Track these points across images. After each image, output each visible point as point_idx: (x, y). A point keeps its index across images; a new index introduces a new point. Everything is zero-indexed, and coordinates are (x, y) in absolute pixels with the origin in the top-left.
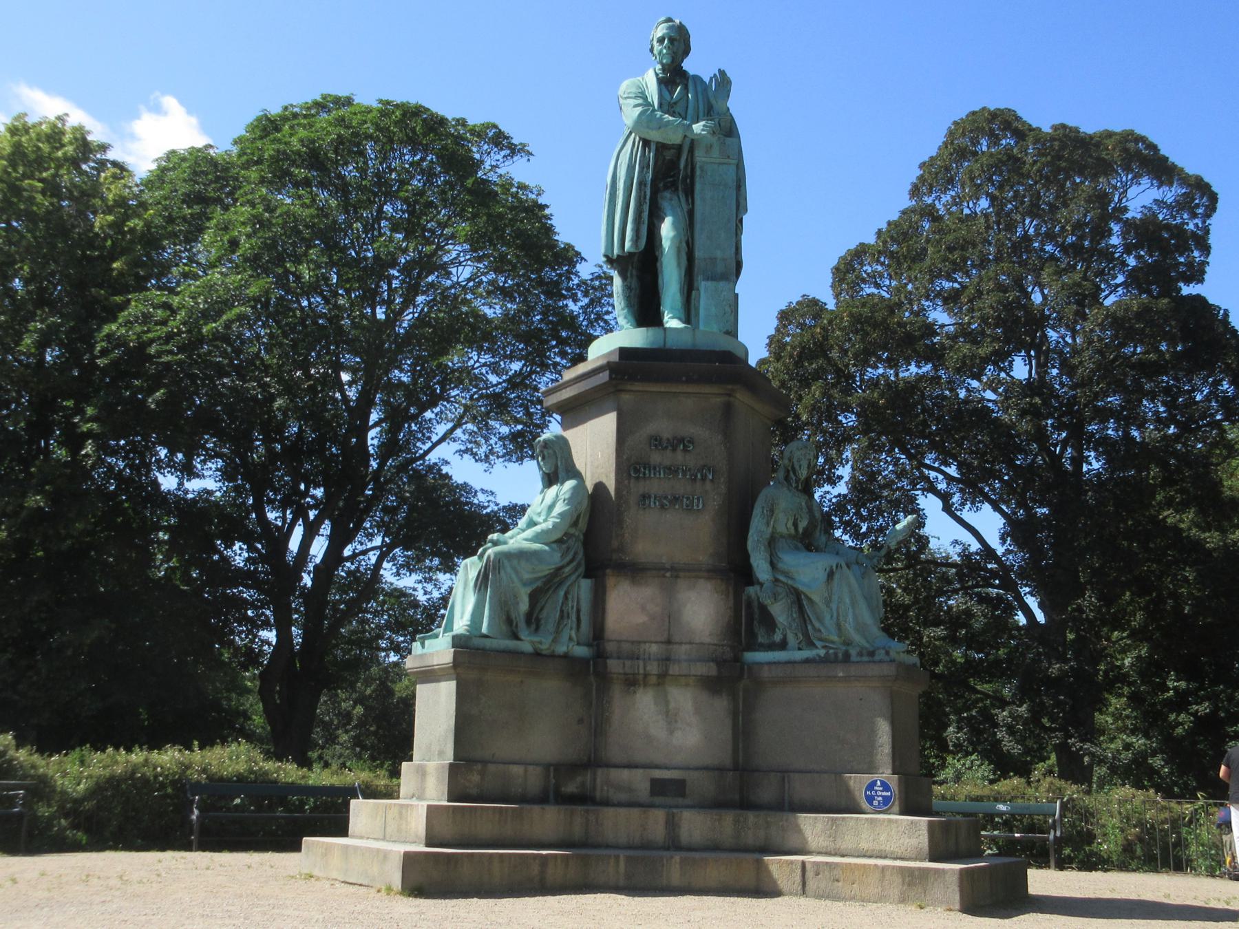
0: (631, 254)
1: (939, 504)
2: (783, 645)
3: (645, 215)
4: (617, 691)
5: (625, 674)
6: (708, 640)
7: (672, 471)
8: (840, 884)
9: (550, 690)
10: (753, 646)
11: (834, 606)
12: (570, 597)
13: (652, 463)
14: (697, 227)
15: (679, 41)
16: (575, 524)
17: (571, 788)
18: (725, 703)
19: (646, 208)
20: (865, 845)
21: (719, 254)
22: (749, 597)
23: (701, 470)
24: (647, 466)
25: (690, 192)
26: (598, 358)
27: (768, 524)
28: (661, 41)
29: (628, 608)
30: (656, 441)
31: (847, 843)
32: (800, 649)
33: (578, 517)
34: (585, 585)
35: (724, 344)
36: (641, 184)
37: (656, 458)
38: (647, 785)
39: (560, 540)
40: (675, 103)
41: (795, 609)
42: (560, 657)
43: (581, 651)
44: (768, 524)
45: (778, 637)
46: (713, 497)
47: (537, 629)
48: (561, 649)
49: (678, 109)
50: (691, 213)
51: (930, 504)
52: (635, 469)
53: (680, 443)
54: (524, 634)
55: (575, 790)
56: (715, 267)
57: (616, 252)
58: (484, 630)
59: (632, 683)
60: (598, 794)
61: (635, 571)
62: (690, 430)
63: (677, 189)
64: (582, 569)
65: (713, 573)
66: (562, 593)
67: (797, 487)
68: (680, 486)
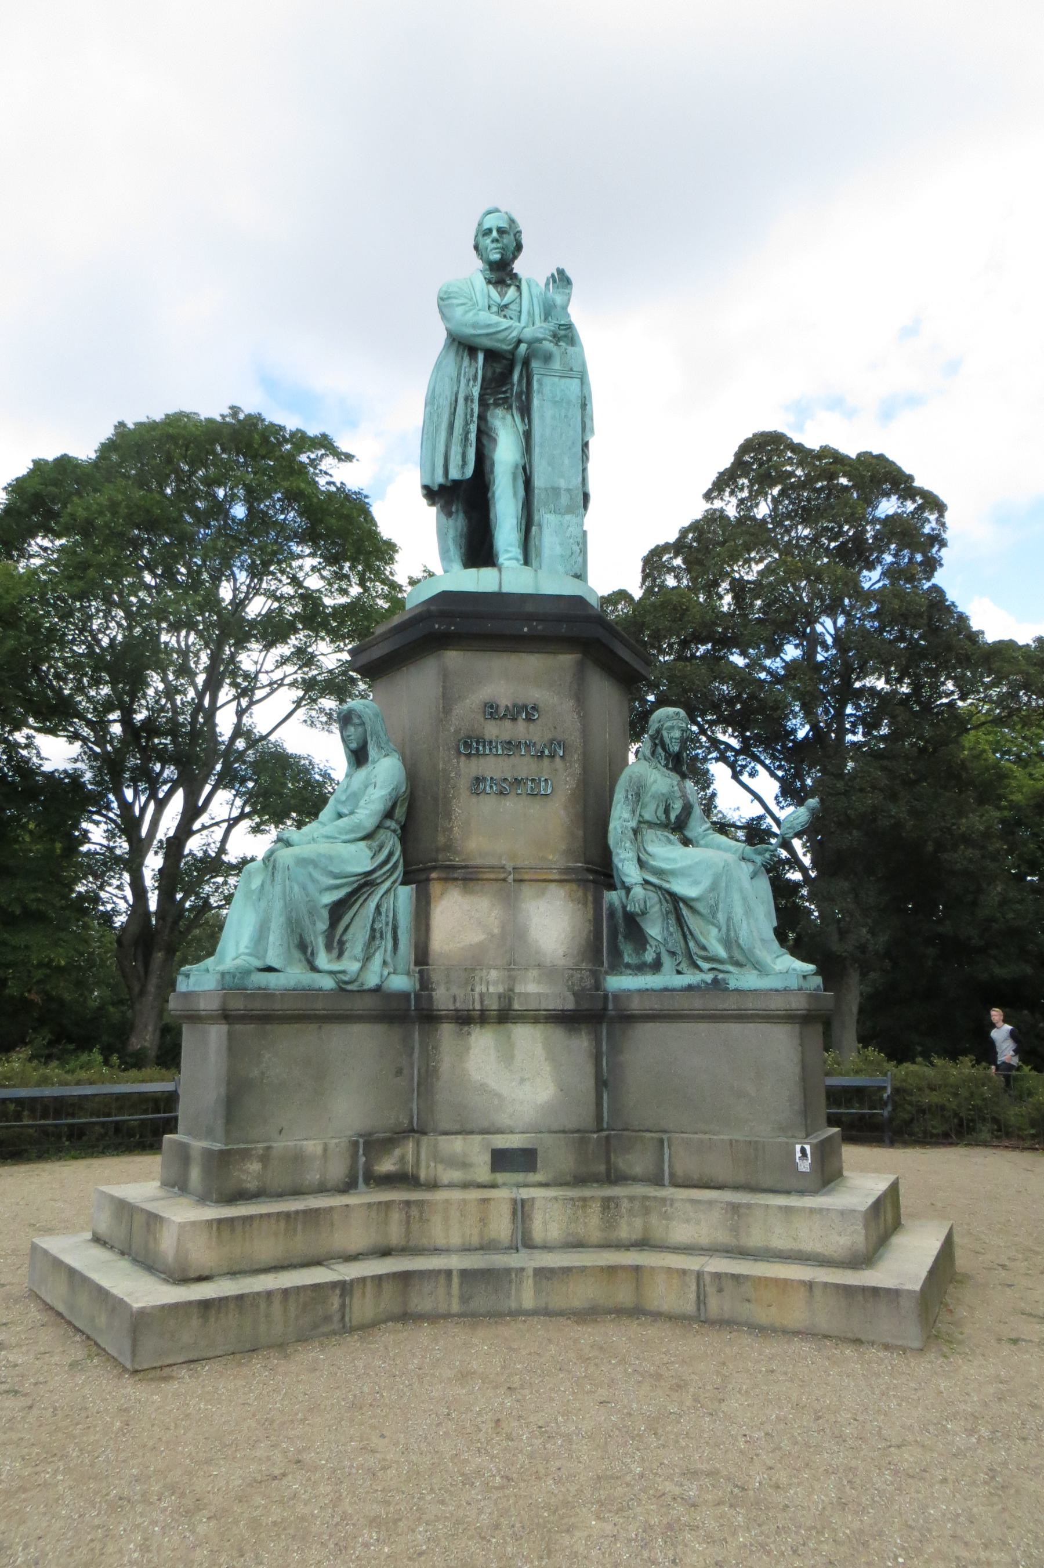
0: (455, 482)
1: (729, 772)
2: (656, 966)
3: (473, 437)
5: (456, 1010)
6: (562, 962)
7: (512, 746)
10: (617, 966)
11: (721, 917)
12: (383, 910)
13: (487, 738)
14: (537, 451)
17: (387, 1166)
19: (473, 428)
20: (779, 1241)
21: (562, 483)
22: (611, 905)
25: (526, 411)
26: (417, 606)
27: (633, 812)
29: (459, 921)
31: (755, 1238)
32: (679, 972)
34: (405, 894)
35: (568, 588)
36: (468, 399)
37: (492, 730)
38: (487, 1158)
40: (506, 306)
41: (672, 921)
42: (371, 991)
43: (400, 983)
45: (649, 956)
46: (563, 779)
47: (340, 955)
48: (372, 980)
50: (528, 435)
51: (719, 771)
52: (466, 743)
53: (527, 712)
54: (323, 960)
56: (559, 497)
59: (465, 1019)
60: (423, 1175)
61: (467, 876)
62: (535, 694)
63: (510, 407)
65: (567, 877)
66: (372, 904)
68: (524, 766)
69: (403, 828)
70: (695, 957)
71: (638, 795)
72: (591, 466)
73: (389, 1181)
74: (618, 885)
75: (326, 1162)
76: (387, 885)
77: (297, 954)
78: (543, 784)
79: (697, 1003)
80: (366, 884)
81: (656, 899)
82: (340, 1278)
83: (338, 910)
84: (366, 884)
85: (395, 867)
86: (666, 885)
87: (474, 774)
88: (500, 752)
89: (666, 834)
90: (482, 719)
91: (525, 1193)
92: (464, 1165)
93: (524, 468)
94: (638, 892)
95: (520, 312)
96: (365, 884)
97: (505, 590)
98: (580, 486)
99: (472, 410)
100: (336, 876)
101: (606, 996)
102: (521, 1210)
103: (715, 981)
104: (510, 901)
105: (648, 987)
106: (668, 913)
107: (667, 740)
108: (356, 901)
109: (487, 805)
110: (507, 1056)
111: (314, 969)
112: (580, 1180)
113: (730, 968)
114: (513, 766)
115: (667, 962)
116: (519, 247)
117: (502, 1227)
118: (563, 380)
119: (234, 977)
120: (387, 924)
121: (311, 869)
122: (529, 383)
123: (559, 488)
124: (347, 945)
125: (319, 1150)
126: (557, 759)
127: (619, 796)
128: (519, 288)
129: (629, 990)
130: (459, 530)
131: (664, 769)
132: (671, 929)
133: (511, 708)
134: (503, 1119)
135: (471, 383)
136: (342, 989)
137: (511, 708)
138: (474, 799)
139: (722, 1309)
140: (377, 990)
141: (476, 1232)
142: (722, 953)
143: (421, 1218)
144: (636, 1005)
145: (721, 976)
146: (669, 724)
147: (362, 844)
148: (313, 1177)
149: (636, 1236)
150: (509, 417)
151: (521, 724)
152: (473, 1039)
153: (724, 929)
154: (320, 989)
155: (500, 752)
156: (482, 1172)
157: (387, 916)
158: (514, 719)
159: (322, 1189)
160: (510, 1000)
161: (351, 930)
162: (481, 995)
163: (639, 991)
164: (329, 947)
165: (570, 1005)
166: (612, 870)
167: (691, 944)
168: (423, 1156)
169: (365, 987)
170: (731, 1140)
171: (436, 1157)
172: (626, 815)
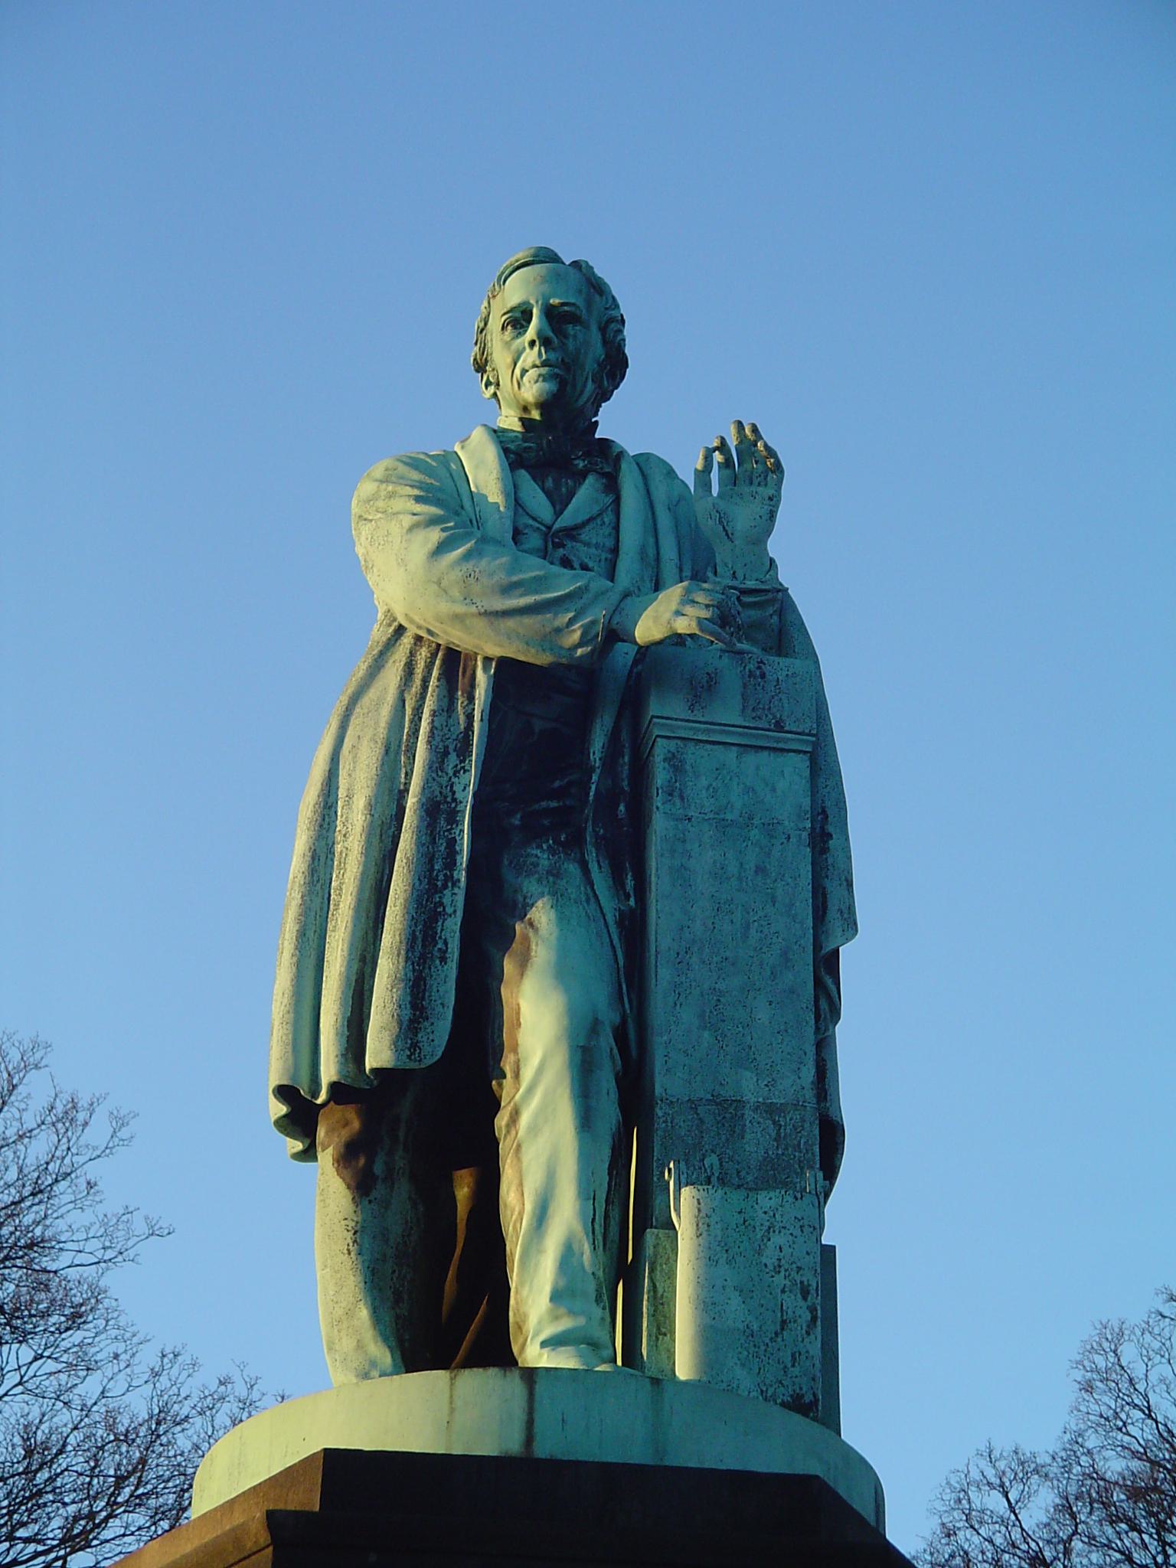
3: (452, 928)
14: (662, 978)
15: (583, 336)
19: (455, 900)
21: (749, 1087)
25: (628, 855)
28: (518, 319)
40: (572, 532)
49: (580, 552)
56: (733, 1115)
57: (329, 1071)
72: (843, 1033)
95: (615, 551)
97: (543, 1449)
98: (810, 1095)
99: (452, 843)
116: (615, 366)
118: (751, 758)
122: (641, 770)
123: (740, 1103)
128: (612, 485)
135: (453, 759)
150: (572, 868)
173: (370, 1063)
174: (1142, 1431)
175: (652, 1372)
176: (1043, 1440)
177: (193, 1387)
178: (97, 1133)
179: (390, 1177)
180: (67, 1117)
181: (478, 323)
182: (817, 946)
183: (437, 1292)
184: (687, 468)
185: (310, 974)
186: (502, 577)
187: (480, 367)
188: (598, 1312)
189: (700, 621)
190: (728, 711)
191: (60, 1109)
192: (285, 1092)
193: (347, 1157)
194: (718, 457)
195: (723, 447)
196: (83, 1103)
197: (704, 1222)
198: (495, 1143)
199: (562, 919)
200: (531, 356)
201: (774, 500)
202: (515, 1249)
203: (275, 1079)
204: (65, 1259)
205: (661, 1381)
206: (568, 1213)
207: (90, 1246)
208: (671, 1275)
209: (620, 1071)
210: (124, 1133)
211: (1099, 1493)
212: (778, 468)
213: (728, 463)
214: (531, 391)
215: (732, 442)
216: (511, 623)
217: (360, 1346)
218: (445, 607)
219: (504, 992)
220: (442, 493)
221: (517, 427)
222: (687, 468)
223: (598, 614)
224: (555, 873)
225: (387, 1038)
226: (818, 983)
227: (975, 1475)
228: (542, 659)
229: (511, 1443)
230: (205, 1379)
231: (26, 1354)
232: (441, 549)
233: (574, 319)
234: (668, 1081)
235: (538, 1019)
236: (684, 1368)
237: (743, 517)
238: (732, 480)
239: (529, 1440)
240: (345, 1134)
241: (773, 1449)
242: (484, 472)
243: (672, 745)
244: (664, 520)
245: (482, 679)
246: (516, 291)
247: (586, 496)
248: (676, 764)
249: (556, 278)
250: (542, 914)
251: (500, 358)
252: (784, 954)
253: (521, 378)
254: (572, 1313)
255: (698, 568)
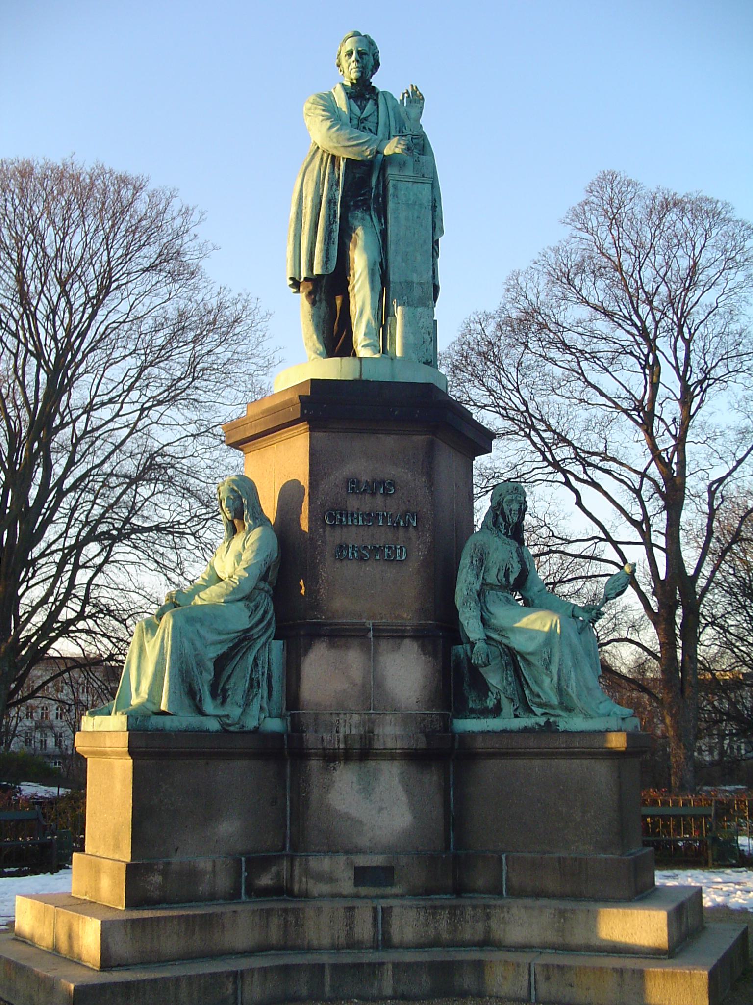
2: (496, 711)
3: (336, 235)
4: (315, 764)
5: (324, 749)
7: (371, 517)
8: (574, 990)
9: (236, 775)
10: (463, 712)
11: (554, 669)
12: (260, 662)
14: (392, 248)
15: (368, 58)
16: (264, 578)
17: (265, 880)
18: (435, 778)
19: (336, 227)
21: (415, 278)
22: (458, 656)
23: (403, 516)
24: (344, 512)
25: (382, 213)
27: (478, 576)
28: (350, 54)
29: (326, 675)
30: (353, 485)
32: (516, 716)
33: (269, 568)
34: (277, 646)
36: (331, 202)
37: (354, 503)
38: (351, 873)
39: (244, 596)
40: (365, 119)
42: (250, 732)
43: (274, 725)
44: (478, 576)
45: (490, 703)
47: (223, 703)
48: (251, 723)
49: (368, 125)
50: (384, 234)
52: (330, 515)
53: (380, 486)
54: (209, 706)
55: (270, 882)
56: (410, 285)
57: (304, 274)
58: (164, 707)
59: (330, 757)
61: (339, 635)
62: (392, 471)
63: (369, 209)
64: (272, 629)
65: (421, 636)
66: (251, 659)
67: (506, 534)
68: (381, 536)
69: (275, 589)
70: (530, 704)
71: (481, 561)
72: (439, 260)
73: (266, 892)
74: (464, 641)
75: (214, 876)
76: (263, 639)
77: (187, 701)
78: (398, 551)
79: (532, 742)
80: (244, 639)
81: (497, 653)
82: (234, 969)
83: (221, 662)
84: (244, 639)
85: (269, 624)
86: (505, 641)
87: (338, 542)
88: (361, 523)
89: (506, 594)
90: (344, 494)
91: (384, 903)
92: (331, 879)
93: (381, 264)
94: (480, 646)
95: (378, 123)
96: (244, 639)
97: (364, 378)
98: (431, 279)
99: (335, 211)
100: (219, 633)
101: (453, 737)
102: (382, 917)
103: (547, 723)
104: (372, 656)
105: (490, 729)
106: (507, 665)
107: (507, 512)
108: (236, 654)
109: (350, 569)
110: (367, 790)
111: (201, 712)
112: (428, 892)
113: (559, 712)
114: (372, 535)
115: (508, 708)
116: (377, 65)
117: (364, 930)
118: (416, 185)
119: (137, 719)
120: (263, 674)
121: (198, 626)
122: (385, 188)
123: (412, 282)
124: (230, 693)
125: (209, 867)
126: (411, 529)
127: (465, 561)
128: (376, 103)
129: (473, 732)
130: (322, 315)
131: (505, 537)
132: (510, 679)
133: (370, 484)
134: (364, 841)
135: (335, 187)
136: (225, 730)
137: (370, 484)
138: (338, 565)
139: (550, 993)
140: (256, 730)
141: (342, 935)
142: (555, 701)
143: (296, 923)
144: (480, 744)
145: (552, 720)
146: (509, 497)
147: (241, 604)
148: (203, 888)
149: (479, 936)
150: (368, 217)
151: (379, 499)
152: (337, 774)
153: (556, 679)
154: (208, 731)
155: (361, 523)
156: (347, 886)
157: (263, 667)
158: (373, 494)
159: (212, 898)
160: (371, 740)
161: (233, 680)
162: (345, 737)
163: (482, 732)
164: (214, 696)
165: (422, 745)
166: (458, 625)
167: (527, 692)
168: (296, 872)
169: (245, 729)
170: (559, 858)
171: (307, 872)
172: (471, 578)
173: (315, 273)
174: (524, 304)
175: (390, 355)
176: (492, 308)
177: (230, 297)
178: (195, 217)
179: (320, 300)
180: (186, 213)
181: (337, 53)
182: (433, 238)
183: (335, 337)
184: (399, 97)
185: (297, 246)
186: (348, 136)
187: (339, 66)
188: (376, 338)
189: (402, 150)
190: (409, 172)
191: (184, 210)
192: (291, 279)
193: (309, 294)
194: (406, 95)
195: (408, 92)
196: (190, 208)
197: (404, 316)
198: (348, 293)
199: (365, 233)
200: (353, 65)
201: (422, 108)
202: (354, 322)
203: (290, 276)
204: (187, 257)
205: (393, 358)
206: (368, 313)
207: (195, 253)
208: (395, 329)
209: (382, 275)
210: (203, 217)
211: (508, 321)
212: (423, 99)
213: (409, 96)
214: (354, 75)
215: (410, 91)
216: (350, 149)
217: (314, 345)
218: (332, 144)
219: (350, 253)
220: (328, 104)
221: (349, 85)
222: (399, 97)
223: (374, 147)
224: (363, 219)
225: (319, 267)
226: (433, 248)
227: (472, 319)
228: (359, 159)
229: (357, 376)
230: (234, 295)
231: (177, 286)
232: (331, 127)
233: (365, 54)
234: (393, 277)
235: (360, 262)
236: (398, 353)
237: (413, 113)
238: (410, 101)
239: (361, 375)
240: (308, 290)
241: (420, 375)
242: (341, 101)
243: (394, 182)
244: (391, 114)
245: (342, 164)
246: (349, 45)
247: (370, 105)
248: (395, 187)
249: (360, 41)
250: (360, 231)
251: (344, 64)
252: (425, 242)
253: (350, 72)
254: (370, 339)
255: (401, 133)
